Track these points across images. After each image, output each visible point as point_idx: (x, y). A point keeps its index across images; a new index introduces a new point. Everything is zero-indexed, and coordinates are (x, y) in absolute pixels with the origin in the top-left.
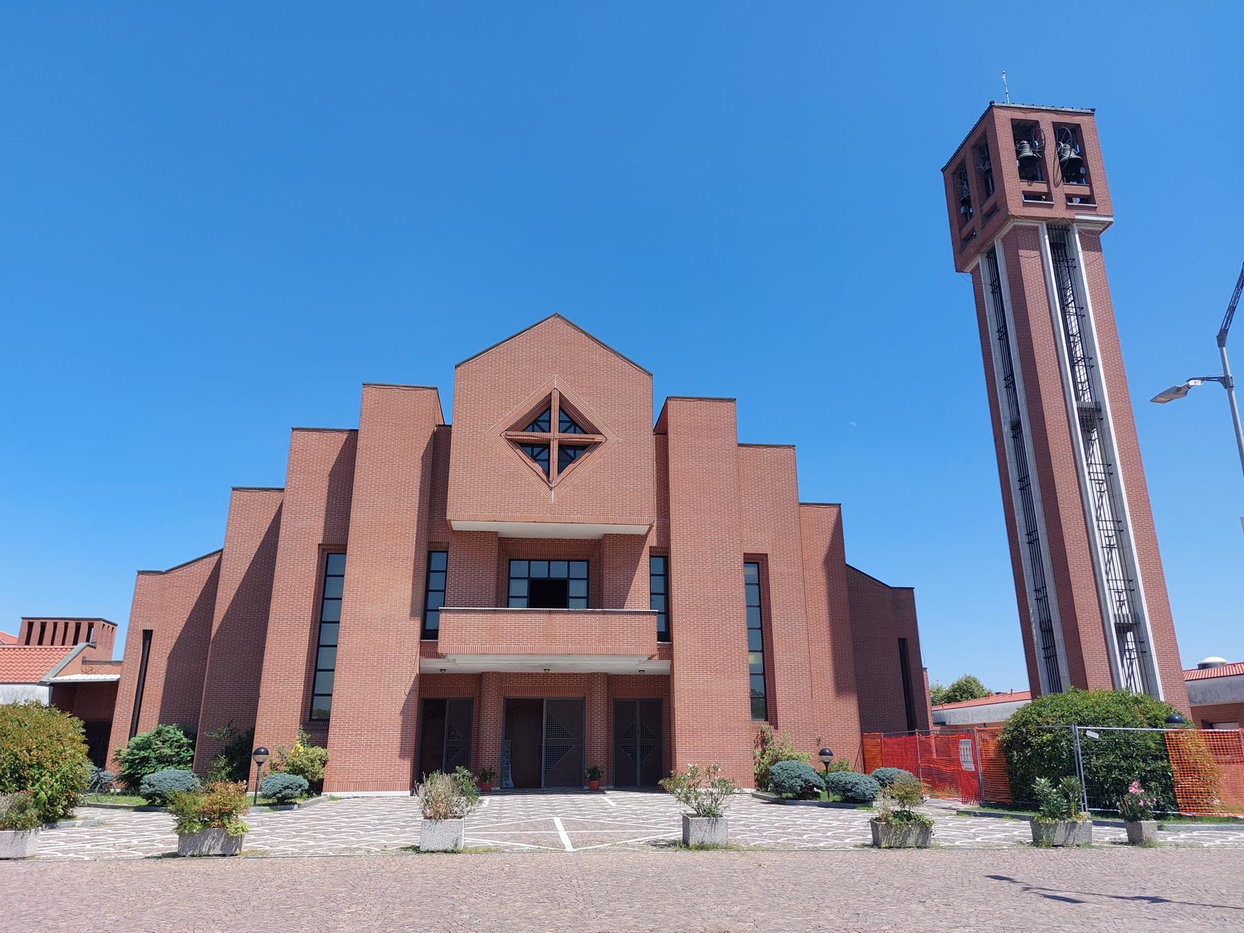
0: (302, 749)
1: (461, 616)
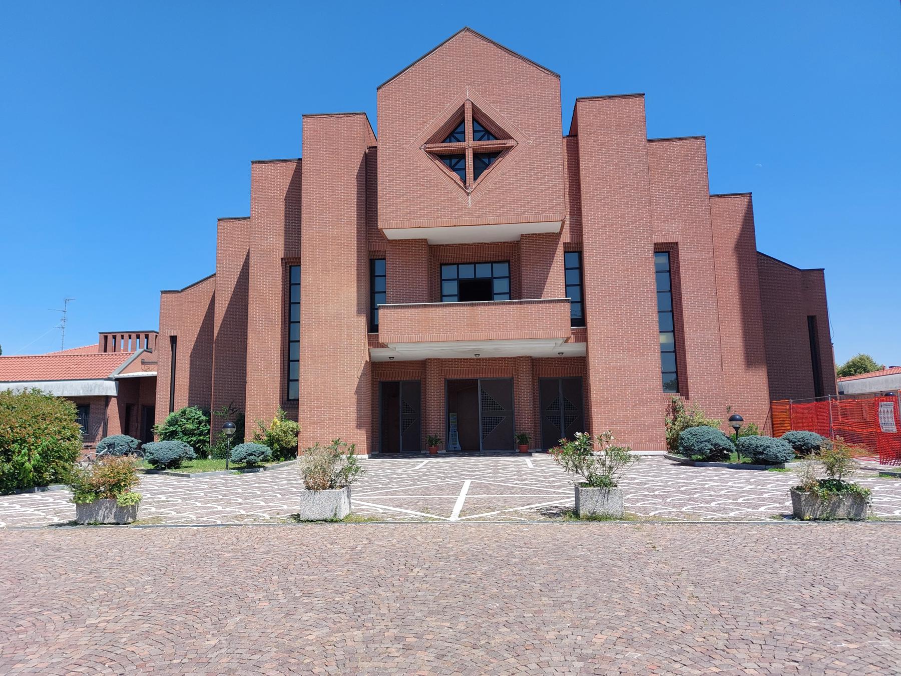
0: (278, 423)
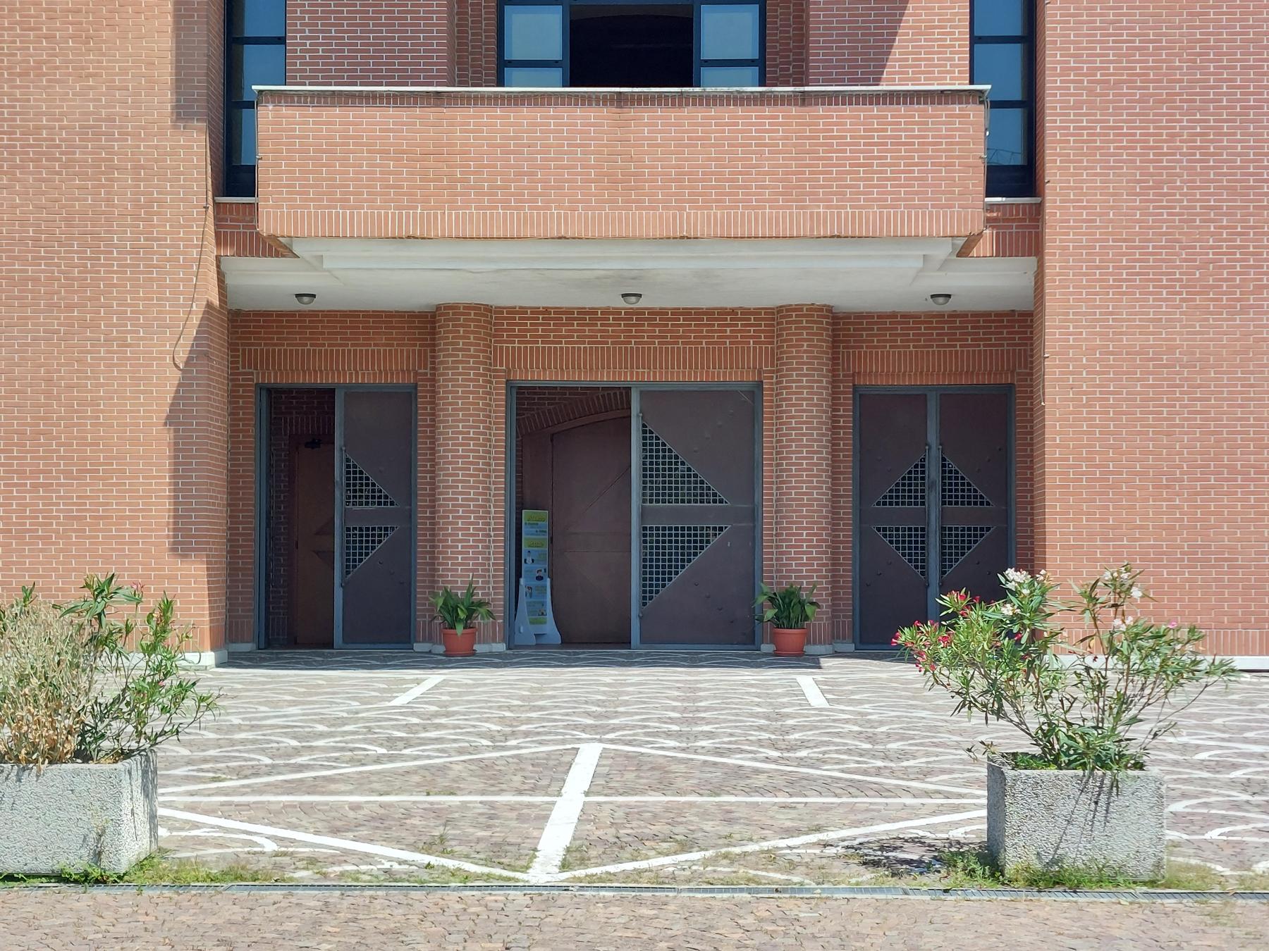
1: (351, 113)
